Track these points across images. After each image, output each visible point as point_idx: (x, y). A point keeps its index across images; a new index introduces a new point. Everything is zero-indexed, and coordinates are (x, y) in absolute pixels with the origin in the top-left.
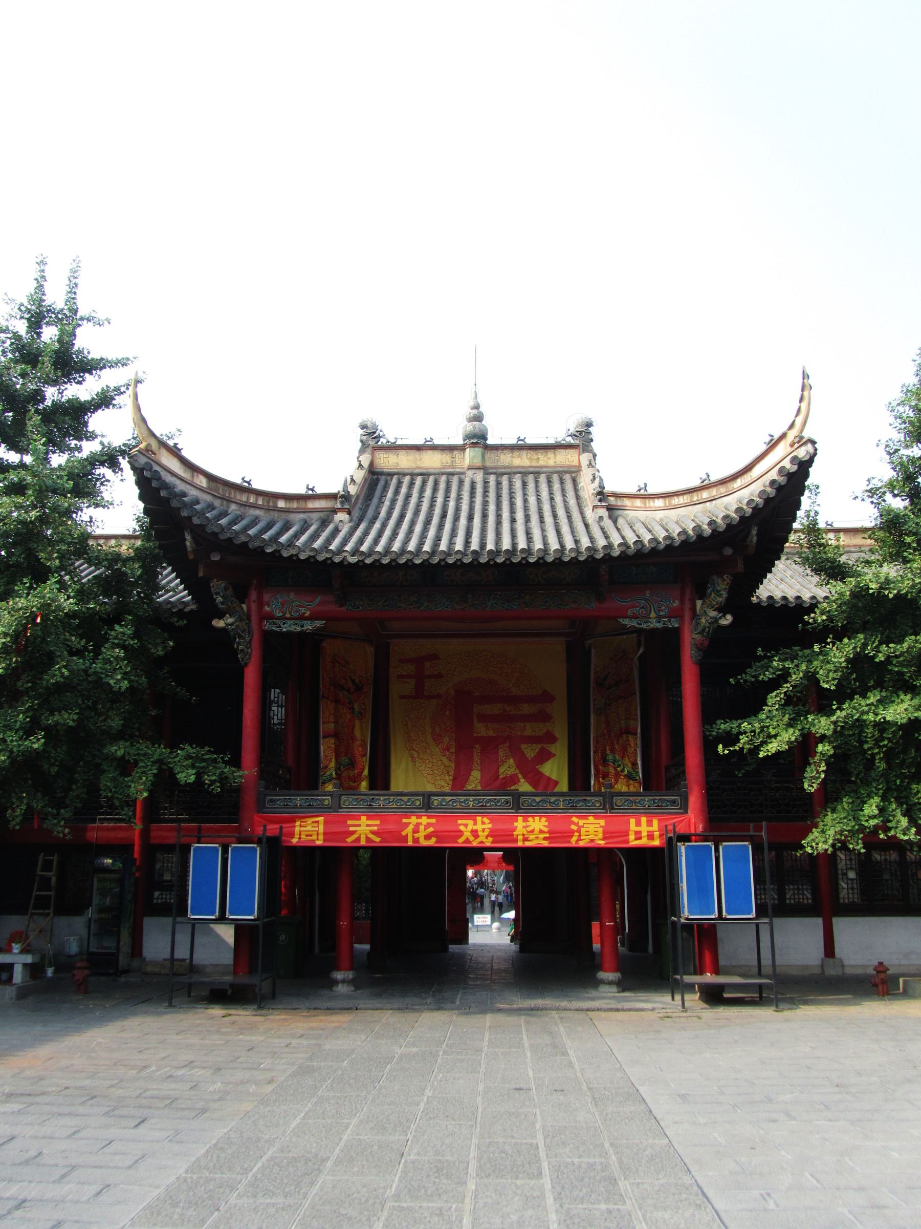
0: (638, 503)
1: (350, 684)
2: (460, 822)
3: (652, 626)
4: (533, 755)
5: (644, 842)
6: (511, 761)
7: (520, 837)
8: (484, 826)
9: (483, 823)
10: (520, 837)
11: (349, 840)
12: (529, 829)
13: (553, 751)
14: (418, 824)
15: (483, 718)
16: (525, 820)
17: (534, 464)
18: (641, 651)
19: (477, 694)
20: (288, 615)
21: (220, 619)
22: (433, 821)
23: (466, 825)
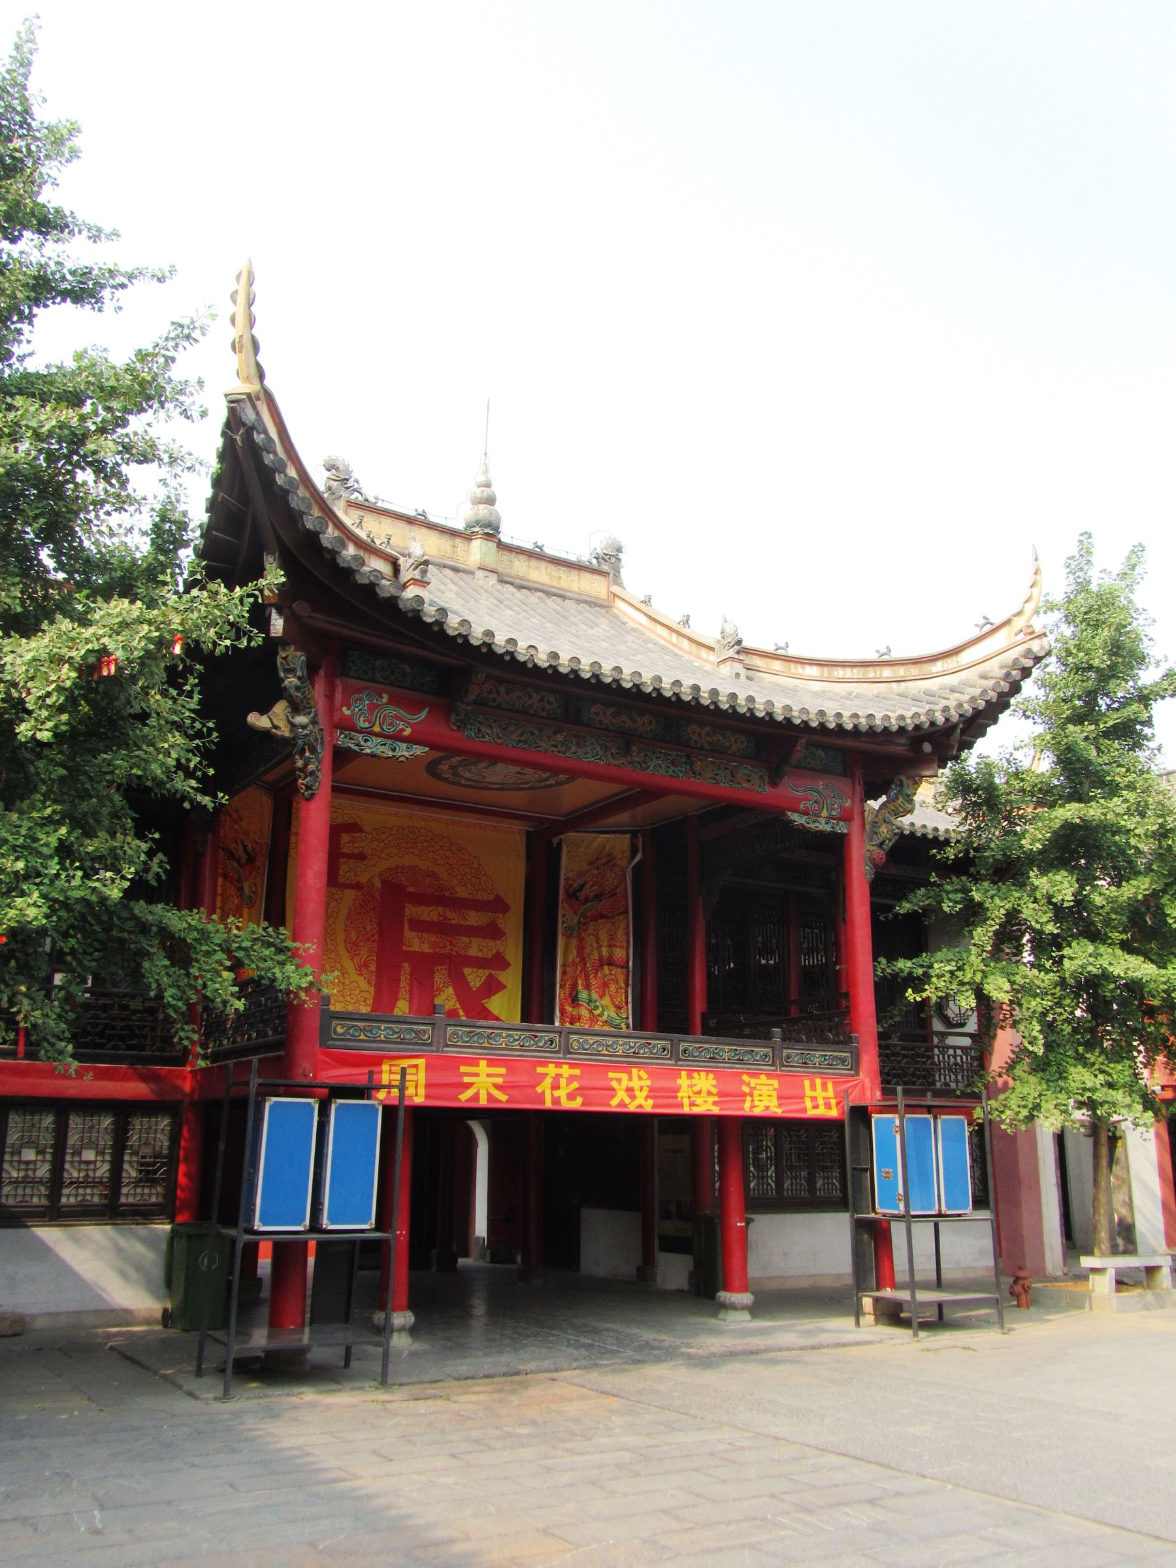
0: (777, 665)
1: (241, 851)
2: (611, 1075)
3: (820, 827)
5: (821, 1112)
6: (450, 990)
8: (643, 1083)
9: (640, 1078)
10: (686, 1101)
11: (465, 1096)
12: (696, 1089)
13: (503, 981)
14: (559, 1076)
15: (419, 926)
16: (690, 1077)
17: (555, 584)
18: (639, 857)
19: (411, 889)
20: (377, 729)
21: (262, 714)
22: (577, 1072)
23: (619, 1081)
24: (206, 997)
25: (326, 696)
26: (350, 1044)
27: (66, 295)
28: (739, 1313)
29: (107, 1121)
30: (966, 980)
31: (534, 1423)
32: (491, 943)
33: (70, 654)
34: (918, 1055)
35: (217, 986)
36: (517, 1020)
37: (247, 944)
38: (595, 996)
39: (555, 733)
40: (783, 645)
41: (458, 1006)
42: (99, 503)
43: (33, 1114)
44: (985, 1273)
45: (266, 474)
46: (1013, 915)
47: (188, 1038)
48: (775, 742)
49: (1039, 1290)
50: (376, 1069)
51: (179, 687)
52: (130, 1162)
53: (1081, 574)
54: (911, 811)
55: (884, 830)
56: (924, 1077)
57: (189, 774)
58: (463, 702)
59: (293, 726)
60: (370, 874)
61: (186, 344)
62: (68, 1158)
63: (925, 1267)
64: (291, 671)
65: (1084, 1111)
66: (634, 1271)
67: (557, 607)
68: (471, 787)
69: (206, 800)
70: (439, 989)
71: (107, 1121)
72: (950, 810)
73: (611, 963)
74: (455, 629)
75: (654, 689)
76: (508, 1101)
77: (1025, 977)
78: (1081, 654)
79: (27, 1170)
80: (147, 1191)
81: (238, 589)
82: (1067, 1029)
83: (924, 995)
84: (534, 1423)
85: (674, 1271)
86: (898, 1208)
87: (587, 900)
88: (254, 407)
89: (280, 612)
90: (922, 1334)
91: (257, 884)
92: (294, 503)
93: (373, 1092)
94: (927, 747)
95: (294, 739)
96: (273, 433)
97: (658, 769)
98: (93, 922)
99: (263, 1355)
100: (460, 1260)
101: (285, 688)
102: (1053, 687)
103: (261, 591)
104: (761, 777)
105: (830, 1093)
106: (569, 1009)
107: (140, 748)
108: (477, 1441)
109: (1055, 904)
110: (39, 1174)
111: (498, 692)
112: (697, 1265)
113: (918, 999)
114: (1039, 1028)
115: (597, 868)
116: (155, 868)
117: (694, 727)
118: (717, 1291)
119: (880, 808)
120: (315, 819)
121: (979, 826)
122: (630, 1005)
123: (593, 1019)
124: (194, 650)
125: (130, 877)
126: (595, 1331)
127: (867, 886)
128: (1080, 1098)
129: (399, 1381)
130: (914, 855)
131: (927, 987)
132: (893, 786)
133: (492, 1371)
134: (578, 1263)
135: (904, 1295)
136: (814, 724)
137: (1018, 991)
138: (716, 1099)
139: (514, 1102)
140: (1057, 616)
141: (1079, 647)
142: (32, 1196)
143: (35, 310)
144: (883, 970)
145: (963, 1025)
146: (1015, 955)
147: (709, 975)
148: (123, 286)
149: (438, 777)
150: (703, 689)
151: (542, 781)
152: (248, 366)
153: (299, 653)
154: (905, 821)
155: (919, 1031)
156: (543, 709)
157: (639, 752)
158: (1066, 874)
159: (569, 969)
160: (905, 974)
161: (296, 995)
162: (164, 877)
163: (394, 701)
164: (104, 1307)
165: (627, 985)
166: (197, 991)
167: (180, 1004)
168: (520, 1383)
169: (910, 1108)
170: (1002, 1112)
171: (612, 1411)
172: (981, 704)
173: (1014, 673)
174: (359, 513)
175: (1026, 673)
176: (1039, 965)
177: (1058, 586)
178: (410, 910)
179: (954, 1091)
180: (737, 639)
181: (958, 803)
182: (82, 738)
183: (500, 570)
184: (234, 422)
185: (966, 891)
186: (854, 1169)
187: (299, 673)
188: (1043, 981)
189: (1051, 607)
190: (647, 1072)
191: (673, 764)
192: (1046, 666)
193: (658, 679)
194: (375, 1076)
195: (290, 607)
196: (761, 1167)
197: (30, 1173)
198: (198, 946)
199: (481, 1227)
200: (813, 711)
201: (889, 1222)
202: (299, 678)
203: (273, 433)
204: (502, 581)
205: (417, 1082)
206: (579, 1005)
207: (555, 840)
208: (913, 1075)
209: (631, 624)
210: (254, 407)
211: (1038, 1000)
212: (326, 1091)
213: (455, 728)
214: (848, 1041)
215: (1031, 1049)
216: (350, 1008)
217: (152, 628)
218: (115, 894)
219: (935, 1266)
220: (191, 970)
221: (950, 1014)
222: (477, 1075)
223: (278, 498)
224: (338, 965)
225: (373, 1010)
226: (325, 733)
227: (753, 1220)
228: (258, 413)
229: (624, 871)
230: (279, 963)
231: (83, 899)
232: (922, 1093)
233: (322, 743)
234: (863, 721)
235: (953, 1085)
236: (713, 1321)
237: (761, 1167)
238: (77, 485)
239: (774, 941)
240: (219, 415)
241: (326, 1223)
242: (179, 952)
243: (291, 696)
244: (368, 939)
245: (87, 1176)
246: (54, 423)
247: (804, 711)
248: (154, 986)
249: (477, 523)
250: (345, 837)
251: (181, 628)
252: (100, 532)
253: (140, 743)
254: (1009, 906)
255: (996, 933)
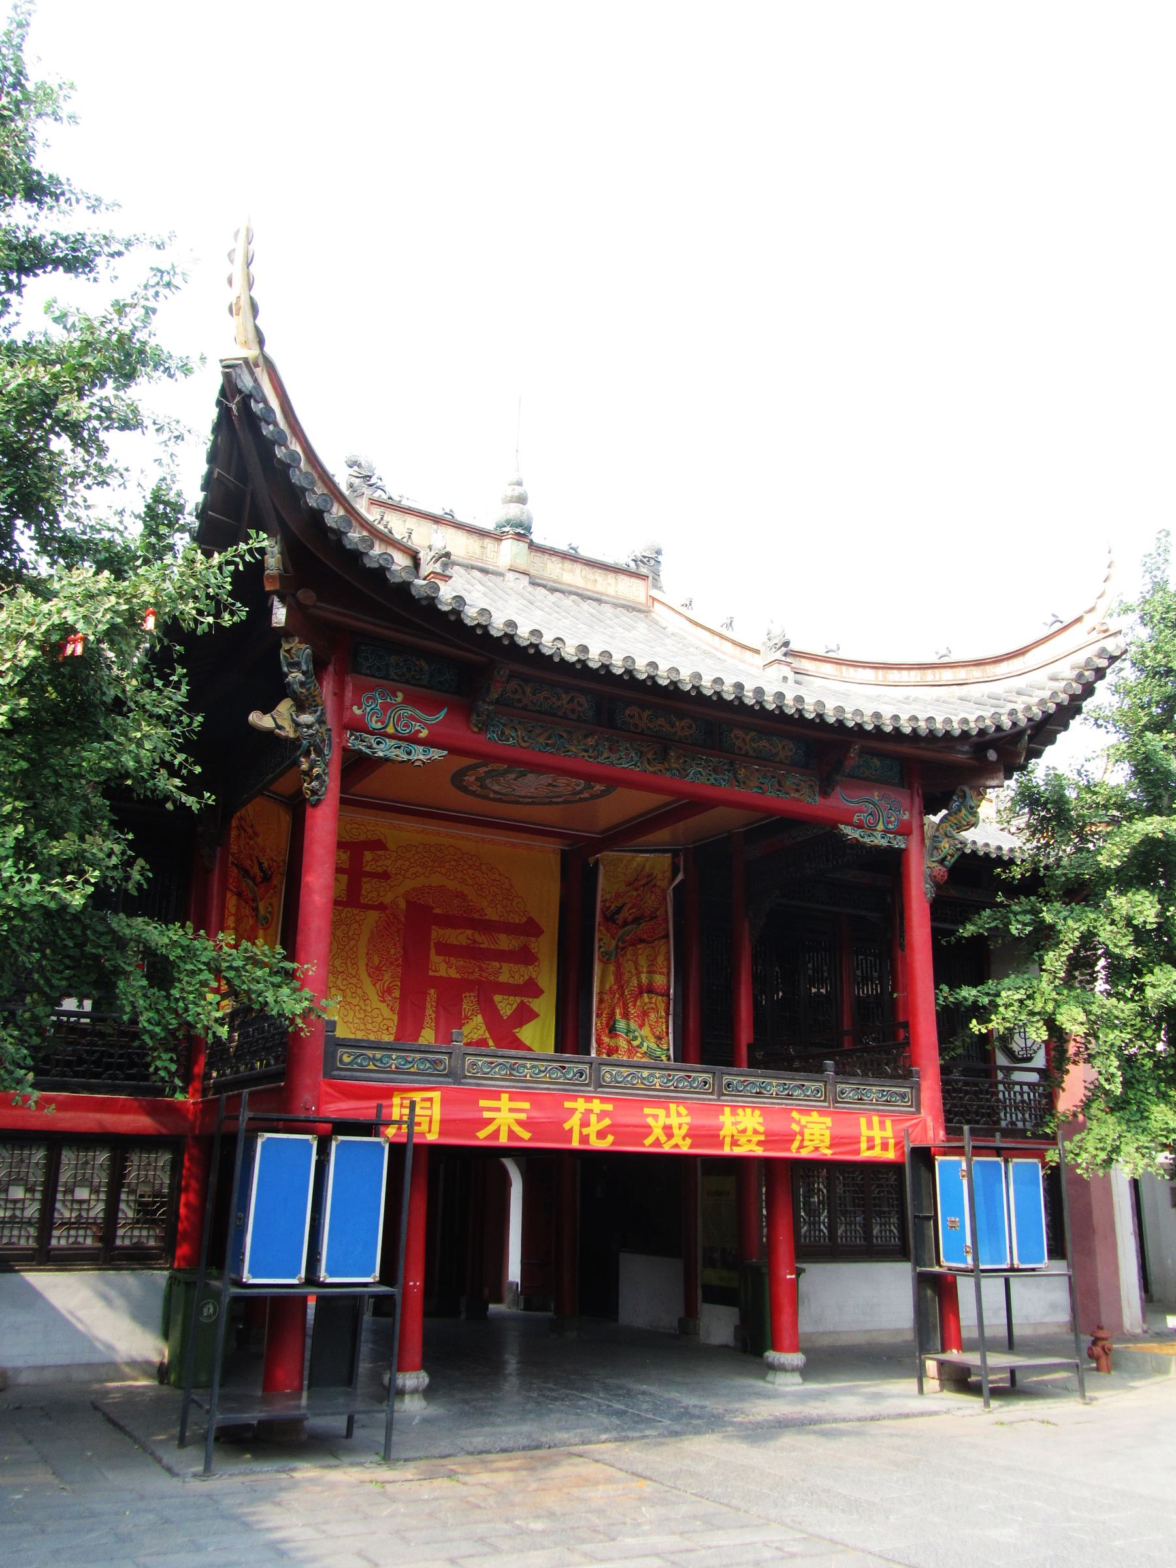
0: (827, 668)
1: (256, 869)
2: (647, 1111)
3: (876, 842)
4: (509, 1012)
5: (877, 1154)
7: (728, 1140)
9: (679, 1114)
11: (482, 1134)
12: (741, 1127)
13: (536, 1009)
15: (445, 950)
16: (734, 1113)
17: (590, 588)
18: (680, 877)
19: (437, 911)
20: (390, 730)
21: (265, 713)
22: (609, 1107)
23: (656, 1117)
24: (188, 1024)
25: (335, 694)
26: (372, 1075)
27: (57, 263)
28: (789, 1374)
29: (103, 1157)
30: (1037, 1010)
31: (551, 1515)
32: (523, 968)
33: (29, 631)
34: (981, 1092)
35: (199, 1010)
36: (551, 1051)
37: (238, 963)
38: (633, 1026)
39: (586, 736)
40: (835, 648)
41: (487, 1035)
42: (78, 476)
43: (87, 1150)
44: (1057, 1330)
45: (265, 447)
46: (1088, 939)
47: (166, 1068)
48: (827, 747)
49: (1117, 1350)
50: (385, 1102)
51: (165, 678)
52: (127, 1201)
53: (1158, 573)
54: (974, 825)
55: (945, 845)
56: (989, 1115)
57: (173, 772)
58: (484, 702)
59: (297, 725)
60: (394, 894)
61: (166, 291)
62: (60, 1196)
63: (995, 1323)
64: (295, 665)
65: (1167, 1153)
66: (675, 1324)
67: (591, 610)
68: (500, 800)
69: (190, 801)
70: (467, 1018)
71: (103, 1157)
72: (1013, 830)
73: (650, 990)
74: (473, 619)
75: (694, 687)
76: (530, 1140)
77: (1102, 1006)
78: (1159, 657)
79: (14, 1209)
80: (145, 1233)
81: (216, 555)
82: (1149, 1064)
83: (990, 1026)
84: (551, 1515)
85: (719, 1325)
86: (965, 1262)
87: (625, 923)
88: (252, 374)
89: (283, 600)
90: (994, 1403)
91: (272, 904)
92: (296, 478)
93: (382, 1128)
94: (992, 755)
95: (298, 739)
96: (274, 403)
97: (699, 778)
98: (64, 936)
99: (255, 1422)
100: (492, 1306)
101: (289, 683)
102: (1127, 693)
103: (242, 557)
104: (811, 786)
105: (889, 1133)
106: (606, 1040)
107: (111, 739)
108: (482, 1540)
109: (1135, 927)
110: (28, 1213)
111: (524, 693)
112: (743, 1319)
113: (984, 1031)
114: (1116, 1063)
115: (637, 890)
116: (136, 876)
117: (738, 732)
118: (764, 1350)
119: (942, 821)
120: (323, 827)
121: (1048, 842)
122: (671, 1036)
123: (632, 1050)
124: (172, 628)
125: (93, 881)
126: (629, 1394)
127: (927, 906)
128: (1165, 1141)
129: (404, 1456)
130: (976, 875)
131: (993, 1017)
132: (955, 798)
133: (511, 1444)
134: (616, 1312)
135: (972, 1359)
136: (869, 727)
137: (1095, 1023)
138: (762, 1138)
139: (619, 1144)
140: (1134, 617)
141: (1156, 650)
142: (19, 1237)
143: (24, 279)
144: (946, 998)
145: (1029, 1059)
146: (1089, 982)
147: (756, 1004)
148: (120, 254)
149: (465, 790)
150: (746, 688)
151: (575, 794)
152: (246, 330)
153: (304, 646)
154: (969, 835)
155: (982, 1065)
156: (573, 711)
157: (678, 758)
158: (1147, 893)
159: (605, 997)
160: (970, 1002)
161: (292, 1021)
162: (145, 887)
163: (409, 700)
164: (95, 1359)
165: (668, 1014)
166: (178, 1015)
167: (158, 1029)
168: (542, 1459)
169: (977, 1151)
170: (1077, 1155)
171: (641, 1499)
172: (1052, 708)
173: (1087, 673)
174: (382, 509)
175: (1100, 673)
176: (1117, 993)
177: (1134, 588)
178: (437, 933)
179: (1025, 1131)
180: (784, 640)
181: (1021, 822)
182: (47, 728)
183: (532, 572)
184: (229, 389)
185: (1035, 912)
186: (916, 1217)
187: (304, 668)
188: (1122, 1011)
189: (1127, 610)
190: (687, 1109)
191: (715, 771)
192: (1121, 670)
193: (698, 676)
194: (384, 1111)
195: (294, 596)
196: (812, 1212)
197: (18, 1213)
198: (181, 964)
199: (514, 1272)
200: (868, 712)
201: (954, 1277)
202: (304, 673)
203: (274, 403)
204: (533, 584)
205: (431, 1117)
206: (616, 1035)
207: (591, 860)
208: (977, 1113)
209: (670, 630)
210: (252, 374)
211: (1117, 1032)
212: (329, 1126)
213: (476, 730)
214: (907, 1075)
215: (1107, 1087)
216: (372, 1037)
217: (121, 601)
218: (77, 900)
219: (1005, 1321)
220: (172, 992)
221: (1016, 1048)
222: (498, 1110)
223: (278, 472)
224: (359, 991)
225: (396, 1039)
226: (334, 734)
227: (803, 1270)
228: (256, 380)
229: (664, 891)
230: (273, 985)
231: (39, 906)
232: (990, 1133)
233: (330, 745)
234: (922, 724)
235: (1020, 1125)
236: (761, 1383)
237: (812, 1212)
238: (51, 453)
239: (825, 968)
240: (214, 382)
241: (324, 1276)
242: (161, 972)
243: (295, 692)
244: (392, 963)
245: (80, 1216)
246: (21, 381)
247: (858, 712)
248: (128, 1009)
249: (508, 522)
250: (368, 855)
251: (152, 601)
252: (75, 504)
253: (111, 732)
254: (1083, 928)
255: (1069, 958)
